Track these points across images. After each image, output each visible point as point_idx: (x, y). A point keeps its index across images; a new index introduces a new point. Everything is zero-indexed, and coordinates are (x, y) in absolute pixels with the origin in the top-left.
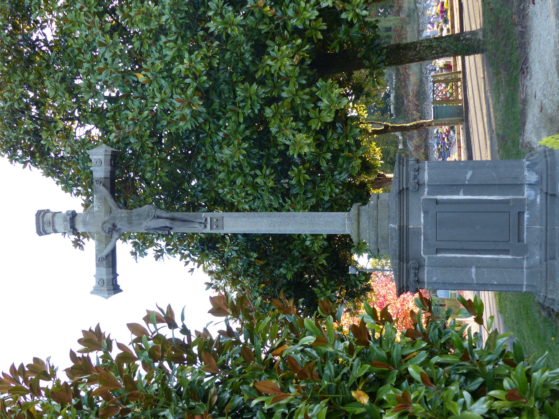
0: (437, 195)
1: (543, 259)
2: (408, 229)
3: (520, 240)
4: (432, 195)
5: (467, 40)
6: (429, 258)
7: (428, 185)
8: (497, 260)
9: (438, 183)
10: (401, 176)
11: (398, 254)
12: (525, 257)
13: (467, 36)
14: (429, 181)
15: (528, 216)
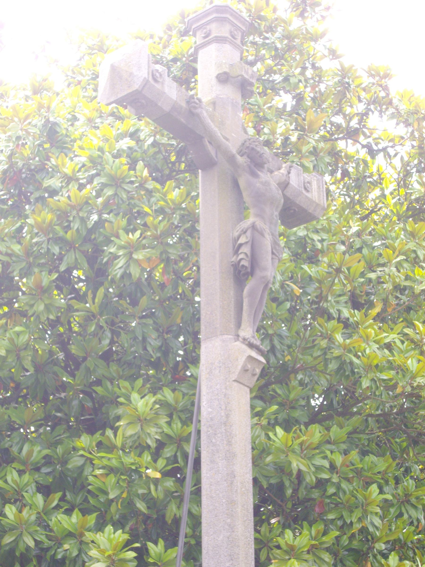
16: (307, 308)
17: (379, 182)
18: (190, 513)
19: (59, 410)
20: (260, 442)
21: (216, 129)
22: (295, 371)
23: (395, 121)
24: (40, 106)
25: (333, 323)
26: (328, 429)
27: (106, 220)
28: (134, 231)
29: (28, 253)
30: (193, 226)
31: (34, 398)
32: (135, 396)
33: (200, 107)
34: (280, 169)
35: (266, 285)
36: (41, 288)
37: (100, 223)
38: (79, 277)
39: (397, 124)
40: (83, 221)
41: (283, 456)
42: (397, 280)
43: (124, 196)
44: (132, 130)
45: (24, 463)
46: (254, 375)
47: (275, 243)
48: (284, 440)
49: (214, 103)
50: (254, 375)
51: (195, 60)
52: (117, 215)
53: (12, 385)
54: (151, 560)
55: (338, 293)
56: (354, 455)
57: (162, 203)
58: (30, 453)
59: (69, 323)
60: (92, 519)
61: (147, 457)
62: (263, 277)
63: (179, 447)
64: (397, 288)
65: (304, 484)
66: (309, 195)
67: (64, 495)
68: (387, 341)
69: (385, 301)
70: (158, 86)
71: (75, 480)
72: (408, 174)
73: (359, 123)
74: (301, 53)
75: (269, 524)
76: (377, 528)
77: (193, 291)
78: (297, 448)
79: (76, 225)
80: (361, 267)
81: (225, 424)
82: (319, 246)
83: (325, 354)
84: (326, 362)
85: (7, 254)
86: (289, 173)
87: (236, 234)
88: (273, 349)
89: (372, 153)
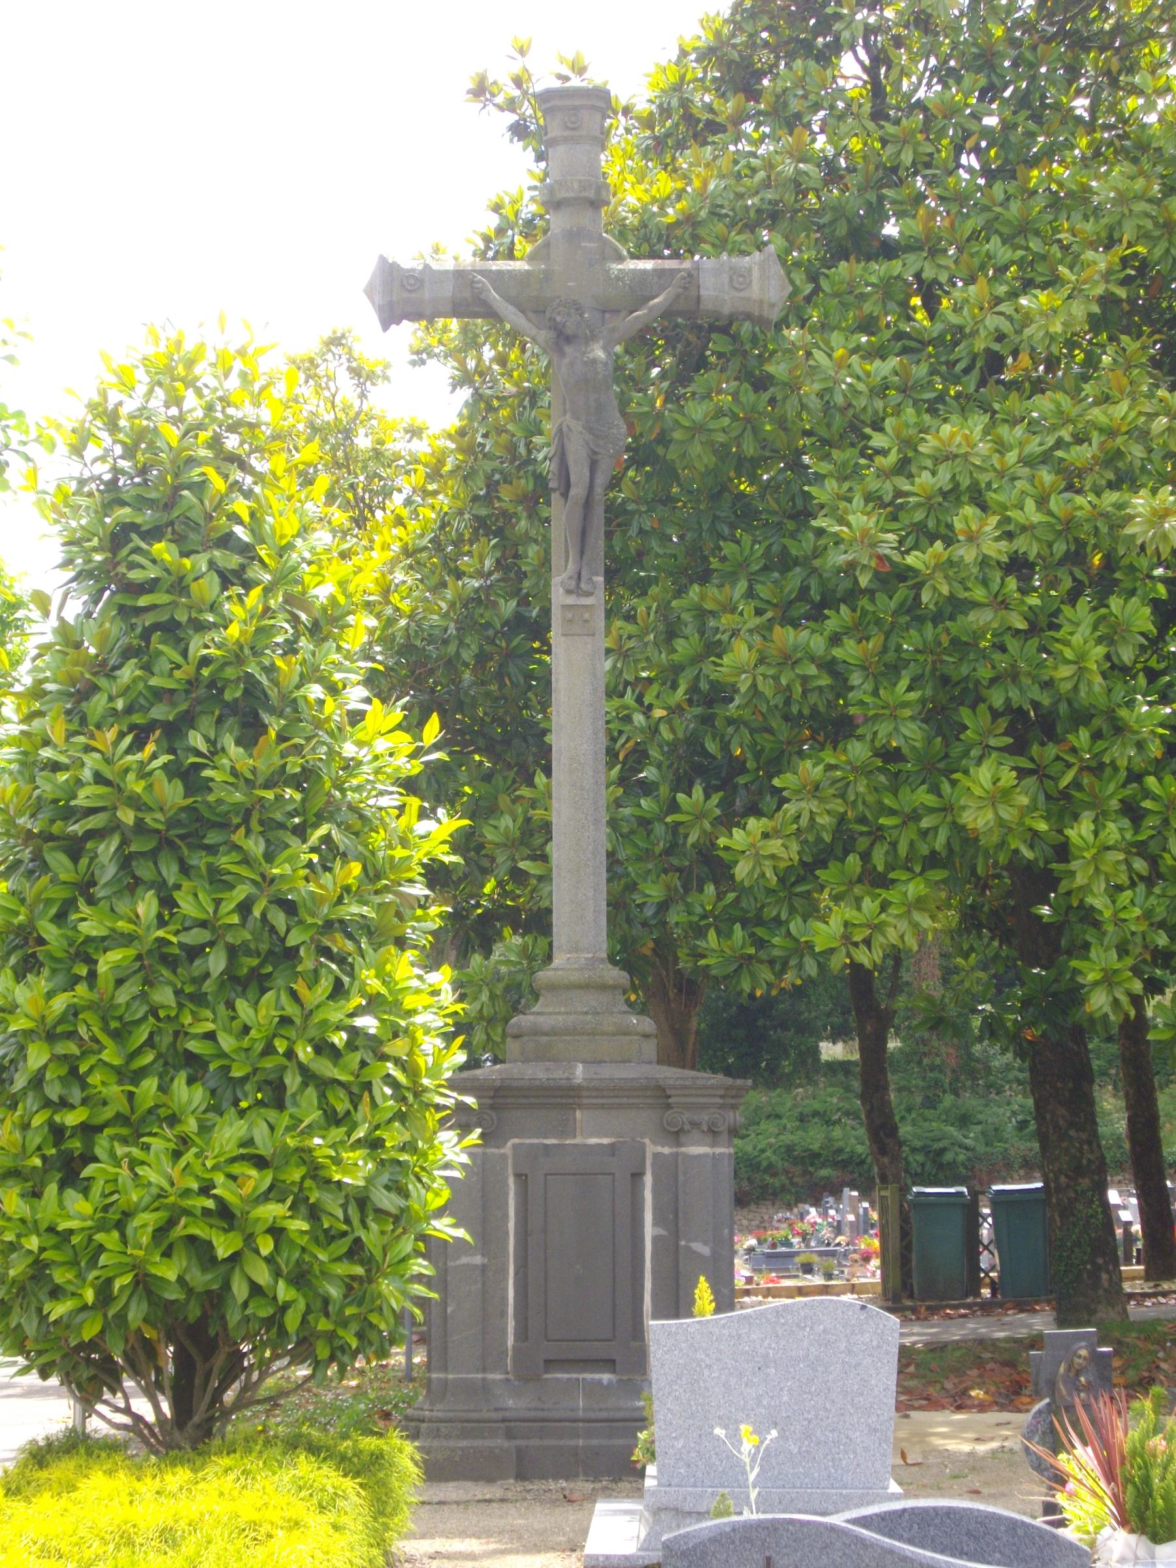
0: (654, 1175)
1: (507, 1414)
2: (572, 1107)
3: (550, 1364)
4: (653, 1164)
5: (1095, 1275)
6: (504, 1157)
7: (677, 1154)
8: (503, 1314)
9: (681, 1178)
10: (710, 1092)
11: (515, 1084)
12: (511, 1376)
13: (1105, 1276)
14: (686, 1156)
15: (605, 1382)
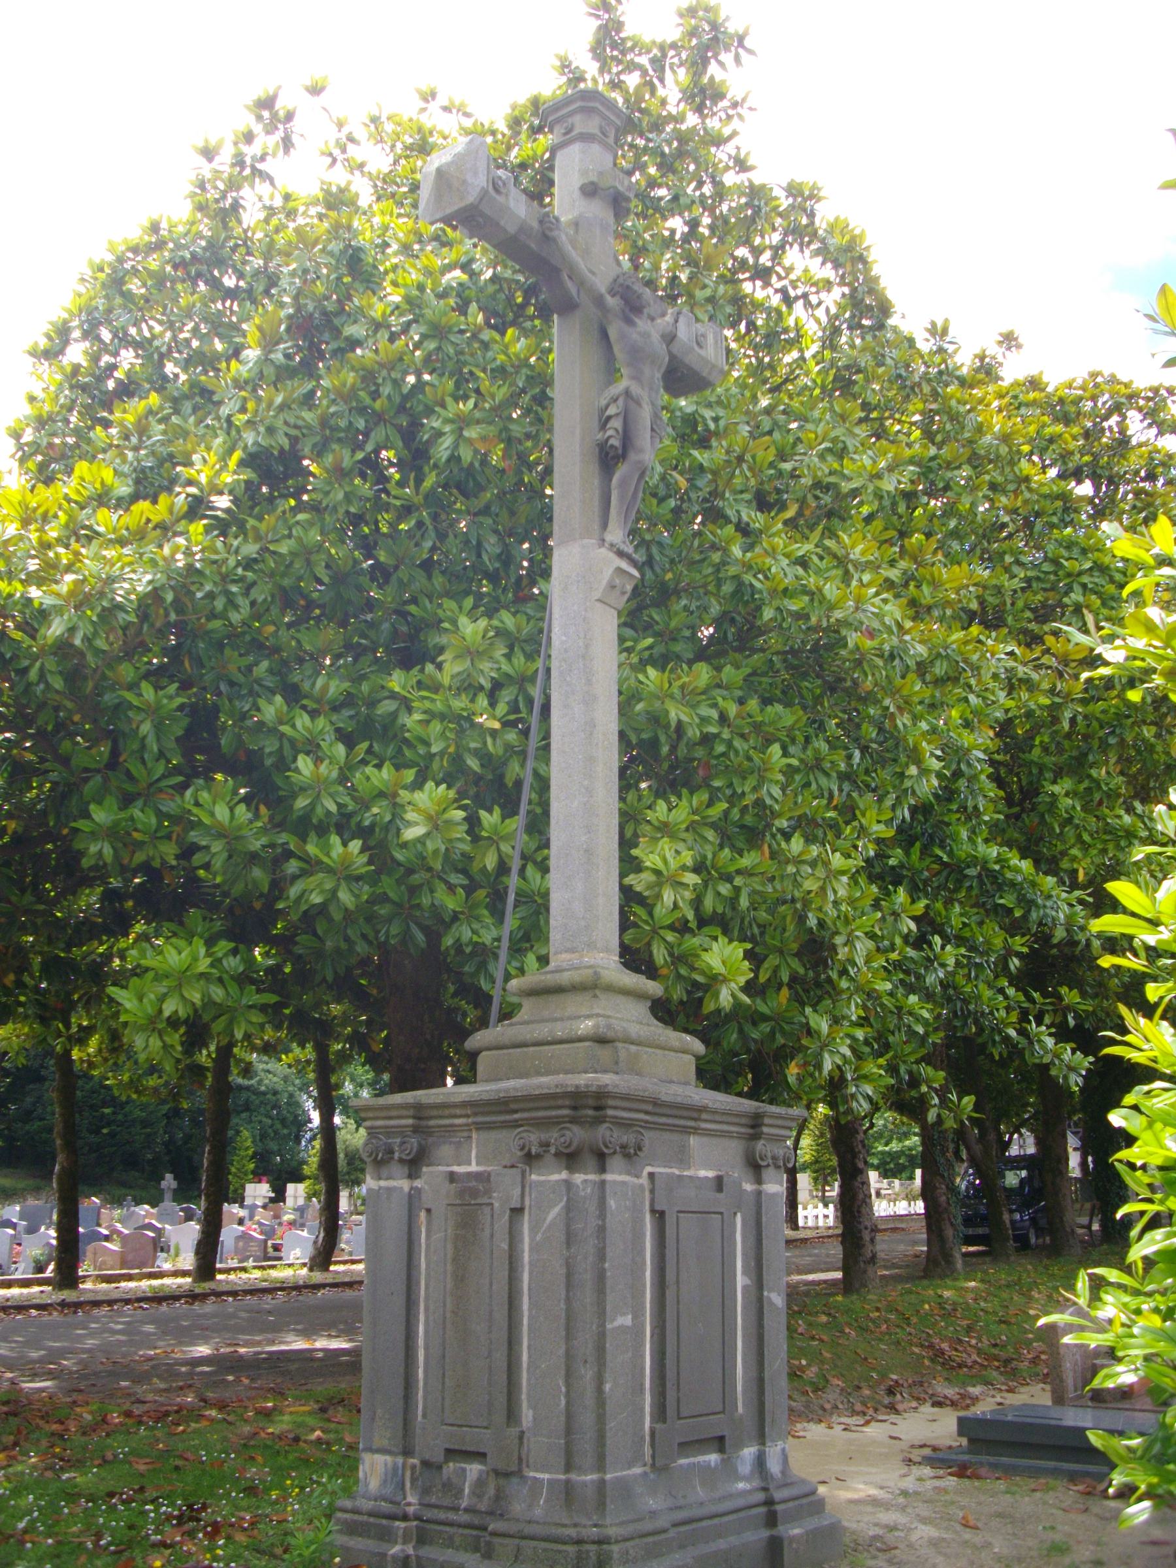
2: (687, 1131)
16: (696, 508)
17: (796, 341)
18: (536, 774)
19: (363, 635)
20: (629, 686)
21: (579, 260)
22: (677, 593)
23: (820, 259)
24: (337, 226)
25: (730, 530)
26: (719, 669)
27: (427, 383)
28: (465, 398)
29: (324, 422)
30: (543, 392)
31: (330, 620)
32: (463, 620)
33: (558, 228)
34: (663, 315)
35: (643, 474)
36: (342, 469)
37: (420, 386)
38: (389, 460)
39: (823, 264)
40: (397, 384)
41: (657, 704)
42: (819, 474)
43: (451, 351)
44: (463, 259)
45: (318, 701)
46: (624, 593)
47: (656, 416)
48: (658, 682)
49: (576, 224)
50: (624, 593)
51: (551, 168)
52: (441, 375)
53: (302, 602)
54: (484, 834)
55: (739, 488)
56: (753, 704)
57: (502, 357)
58: (325, 688)
59: (376, 522)
60: (409, 775)
61: (482, 701)
62: (639, 462)
63: (522, 689)
64: (818, 484)
65: (685, 740)
66: (702, 352)
67: (371, 746)
68: (800, 553)
69: (803, 502)
70: (500, 199)
71: (385, 728)
72: (836, 331)
73: (773, 259)
74: (696, 161)
75: (638, 789)
76: (776, 801)
77: (542, 480)
78: (676, 691)
79: (386, 390)
80: (771, 456)
81: (583, 657)
82: (712, 426)
83: (718, 571)
84: (719, 583)
85: (296, 427)
86: (676, 321)
87: (604, 402)
88: (650, 562)
89: (788, 301)
